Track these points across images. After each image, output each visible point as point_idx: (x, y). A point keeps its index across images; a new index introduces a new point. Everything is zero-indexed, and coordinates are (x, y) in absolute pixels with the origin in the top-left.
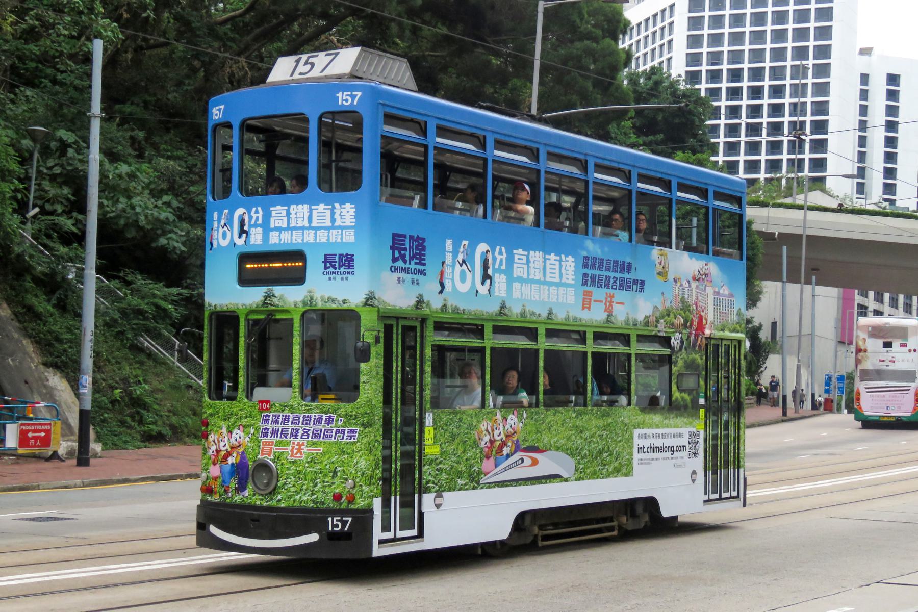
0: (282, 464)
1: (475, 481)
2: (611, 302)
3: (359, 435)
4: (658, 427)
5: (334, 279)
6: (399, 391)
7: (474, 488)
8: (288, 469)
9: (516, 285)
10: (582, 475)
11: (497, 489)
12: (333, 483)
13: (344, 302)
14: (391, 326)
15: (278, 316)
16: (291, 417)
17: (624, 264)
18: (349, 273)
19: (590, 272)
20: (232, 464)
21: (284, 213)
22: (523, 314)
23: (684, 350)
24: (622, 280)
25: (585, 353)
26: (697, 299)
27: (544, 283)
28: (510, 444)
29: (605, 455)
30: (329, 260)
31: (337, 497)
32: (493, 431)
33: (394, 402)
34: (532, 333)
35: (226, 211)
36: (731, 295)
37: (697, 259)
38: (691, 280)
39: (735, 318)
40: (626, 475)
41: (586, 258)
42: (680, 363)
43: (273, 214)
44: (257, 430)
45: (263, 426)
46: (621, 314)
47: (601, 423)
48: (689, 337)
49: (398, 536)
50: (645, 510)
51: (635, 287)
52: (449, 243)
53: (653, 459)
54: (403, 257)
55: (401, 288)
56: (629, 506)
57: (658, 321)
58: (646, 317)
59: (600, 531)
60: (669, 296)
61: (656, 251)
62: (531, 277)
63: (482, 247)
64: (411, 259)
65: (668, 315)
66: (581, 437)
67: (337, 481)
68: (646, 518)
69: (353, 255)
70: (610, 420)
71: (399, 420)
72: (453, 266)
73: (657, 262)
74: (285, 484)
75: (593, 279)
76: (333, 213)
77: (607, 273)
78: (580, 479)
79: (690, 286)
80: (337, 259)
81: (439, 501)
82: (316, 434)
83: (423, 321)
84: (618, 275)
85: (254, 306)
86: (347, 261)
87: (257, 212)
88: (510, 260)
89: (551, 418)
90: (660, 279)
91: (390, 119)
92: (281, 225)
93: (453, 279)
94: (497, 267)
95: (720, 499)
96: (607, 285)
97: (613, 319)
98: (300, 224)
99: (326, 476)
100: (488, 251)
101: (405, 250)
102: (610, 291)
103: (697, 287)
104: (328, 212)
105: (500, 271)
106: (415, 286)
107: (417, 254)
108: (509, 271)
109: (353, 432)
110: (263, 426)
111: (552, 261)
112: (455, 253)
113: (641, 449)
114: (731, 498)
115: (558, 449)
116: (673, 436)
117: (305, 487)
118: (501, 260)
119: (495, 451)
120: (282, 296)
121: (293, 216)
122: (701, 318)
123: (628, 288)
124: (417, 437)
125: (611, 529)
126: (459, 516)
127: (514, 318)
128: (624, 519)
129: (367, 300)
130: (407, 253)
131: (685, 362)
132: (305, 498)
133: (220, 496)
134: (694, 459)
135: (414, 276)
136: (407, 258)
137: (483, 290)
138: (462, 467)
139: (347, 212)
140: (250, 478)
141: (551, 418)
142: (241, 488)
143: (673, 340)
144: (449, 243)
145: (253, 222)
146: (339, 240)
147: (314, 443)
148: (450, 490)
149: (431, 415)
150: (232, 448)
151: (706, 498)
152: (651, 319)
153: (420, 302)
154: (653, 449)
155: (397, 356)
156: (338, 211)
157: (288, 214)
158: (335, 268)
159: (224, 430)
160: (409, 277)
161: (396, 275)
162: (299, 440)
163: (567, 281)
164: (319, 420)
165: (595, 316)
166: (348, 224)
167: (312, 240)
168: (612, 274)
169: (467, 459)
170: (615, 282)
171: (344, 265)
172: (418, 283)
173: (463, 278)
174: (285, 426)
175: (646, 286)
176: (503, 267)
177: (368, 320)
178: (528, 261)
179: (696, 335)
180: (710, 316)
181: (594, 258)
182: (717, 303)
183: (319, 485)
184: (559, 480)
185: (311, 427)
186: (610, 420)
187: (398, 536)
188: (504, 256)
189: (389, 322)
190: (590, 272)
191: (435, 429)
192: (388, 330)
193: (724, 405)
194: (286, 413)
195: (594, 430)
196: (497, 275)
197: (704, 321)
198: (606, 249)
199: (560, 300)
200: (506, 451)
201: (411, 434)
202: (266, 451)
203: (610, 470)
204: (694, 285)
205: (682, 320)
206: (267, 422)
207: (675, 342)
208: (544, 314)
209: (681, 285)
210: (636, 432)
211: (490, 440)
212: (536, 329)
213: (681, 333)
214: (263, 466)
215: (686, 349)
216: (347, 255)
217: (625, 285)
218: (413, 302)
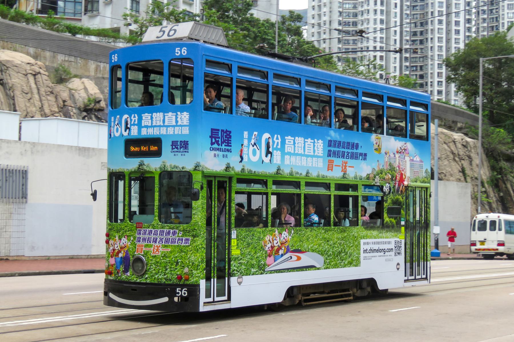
0: (148, 258)
1: (262, 269)
2: (345, 166)
3: (191, 242)
4: (375, 238)
5: (177, 155)
6: (216, 218)
7: (262, 274)
8: (151, 260)
9: (287, 157)
10: (328, 266)
11: (276, 274)
12: (176, 269)
13: (183, 168)
14: (211, 181)
15: (147, 175)
16: (153, 231)
17: (353, 144)
18: (185, 152)
19: (332, 149)
20: (121, 257)
21: (149, 117)
22: (291, 174)
23: (391, 194)
24: (352, 153)
25: (330, 195)
26: (399, 164)
27: (304, 155)
28: (283, 248)
29: (343, 254)
30: (174, 144)
31: (180, 278)
32: (273, 241)
33: (213, 224)
34: (297, 185)
35: (118, 116)
36: (421, 161)
37: (399, 141)
38: (396, 153)
39: (424, 175)
40: (356, 266)
41: (330, 141)
42: (389, 201)
43: (144, 118)
44: (134, 238)
45: (138, 236)
46: (351, 173)
47: (340, 236)
48: (394, 186)
49: (215, 300)
50: (368, 286)
51: (361, 157)
52: (246, 134)
53: (372, 257)
54: (217, 142)
55: (216, 160)
56: (358, 283)
57: (375, 177)
58: (368, 174)
59: (342, 296)
60: (382, 162)
61: (374, 136)
62: (296, 152)
63: (266, 136)
64: (222, 143)
65: (382, 173)
66: (328, 244)
67: (178, 267)
68: (369, 289)
69: (188, 142)
70: (346, 234)
71: (216, 234)
72: (248, 147)
73: (374, 143)
74: (150, 269)
75: (334, 153)
76: (176, 118)
77: (343, 150)
78: (327, 268)
79: (395, 156)
80: (179, 144)
81: (240, 280)
82: (167, 241)
83: (230, 178)
84: (350, 151)
85: (133, 170)
86: (185, 145)
87: (135, 117)
88: (283, 142)
89: (309, 233)
90: (376, 153)
91: (209, 63)
92: (147, 124)
93: (248, 154)
94: (275, 146)
95: (415, 279)
96: (343, 157)
97: (347, 176)
98: (158, 124)
99: (172, 264)
100: (269, 138)
101: (219, 138)
102: (345, 160)
103: (399, 157)
104: (174, 117)
105: (277, 149)
106: (225, 159)
107: (226, 140)
109: (188, 240)
110: (138, 236)
111: (309, 143)
112: (249, 139)
113: (365, 251)
114: (422, 279)
115: (313, 251)
116: (385, 243)
117: (160, 271)
118: (278, 142)
119: (274, 252)
120: (148, 164)
121: (154, 119)
122: (402, 174)
123: (356, 158)
124: (227, 245)
125: (349, 295)
126: (248, 290)
127: (285, 175)
128: (355, 290)
129: (196, 167)
130: (220, 140)
131: (392, 200)
132: (160, 277)
133: (115, 275)
134: (398, 257)
135: (224, 153)
136: (220, 143)
137: (267, 160)
138: (254, 262)
139: (185, 117)
140: (131, 267)
141: (309, 233)
142: (126, 271)
143: (384, 188)
144: (246, 134)
145: (132, 123)
146: (180, 133)
147: (166, 246)
148: (247, 275)
149: (235, 231)
150: (121, 248)
151: (406, 278)
152: (371, 176)
153: (228, 168)
154: (372, 251)
155: (215, 198)
156: (179, 117)
157: (152, 118)
158: (178, 149)
159: (117, 238)
160: (221, 153)
161: (213, 152)
162: (157, 244)
163: (318, 155)
164: (169, 233)
165: (335, 175)
166: (185, 124)
167: (165, 133)
168: (346, 150)
169: (257, 257)
170: (348, 154)
171: (182, 147)
172: (227, 157)
173: (254, 154)
174: (150, 236)
175: (367, 157)
176: (279, 147)
177: (197, 177)
178: (294, 143)
179: (399, 185)
180: (408, 173)
181: (335, 141)
182: (412, 166)
183: (169, 270)
184: (314, 268)
185: (164, 237)
186: (346, 234)
187: (215, 300)
188: (280, 141)
189: (210, 179)
190: (332, 149)
191: (238, 240)
192: (210, 184)
193: (418, 225)
194: (150, 229)
195: (336, 240)
196: (275, 151)
197: (404, 176)
198: (343, 136)
199: (314, 165)
200: (281, 252)
201: (223, 241)
202: (140, 250)
203: (346, 263)
204: (397, 155)
206: (140, 234)
207: (386, 189)
208: (304, 174)
209: (390, 156)
210: (362, 241)
211: (271, 246)
212: (300, 182)
213: (389, 183)
214: (138, 260)
215: (392, 193)
216: (184, 141)
217: (354, 156)
218: (224, 167)
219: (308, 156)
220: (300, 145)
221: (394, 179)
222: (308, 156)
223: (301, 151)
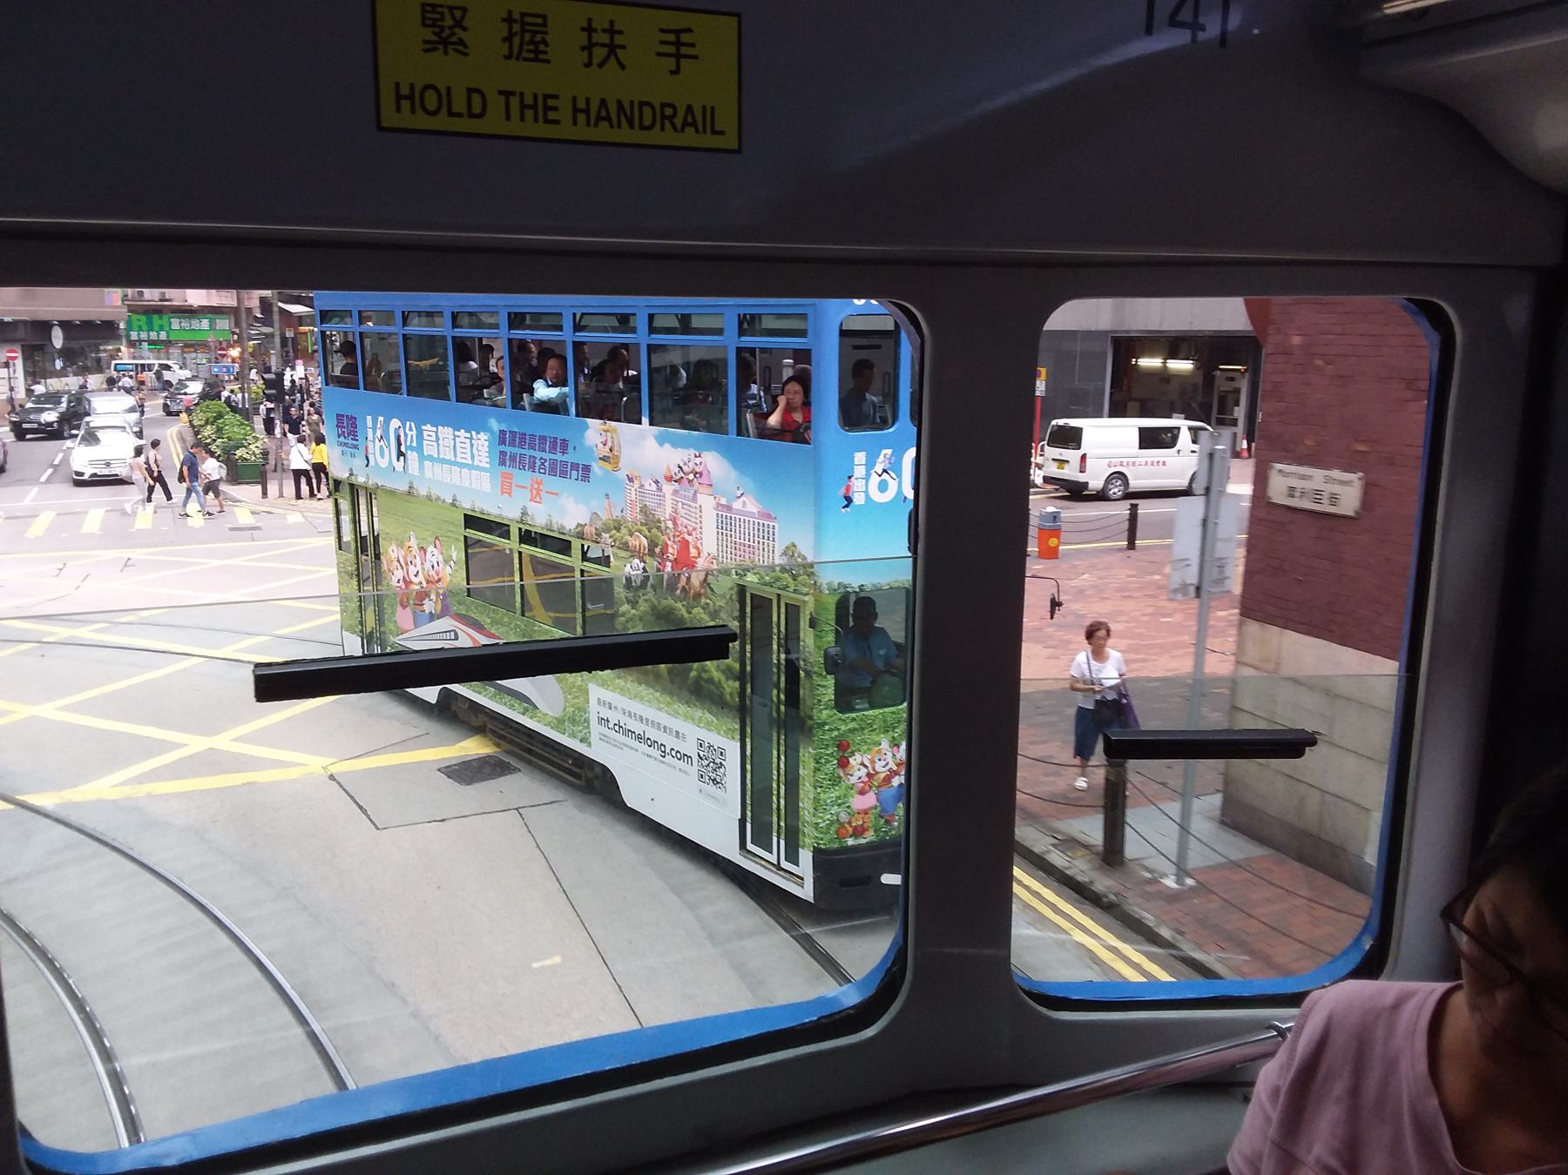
2: (539, 490)
9: (427, 464)
24: (553, 463)
27: (455, 463)
63: (395, 423)
65: (618, 530)
72: (867, 477)
75: (513, 459)
77: (532, 453)
79: (659, 489)
96: (532, 468)
103: (676, 492)
105: (410, 448)
108: (419, 449)
123: (564, 474)
131: (654, 608)
137: (399, 466)
152: (587, 529)
154: (619, 727)
168: (538, 454)
182: (724, 525)
190: (508, 449)
197: (693, 552)
204: (668, 488)
205: (645, 542)
209: (642, 486)
219: (462, 466)
220: (446, 442)
221: (657, 550)
222: (462, 466)
223: (450, 456)
